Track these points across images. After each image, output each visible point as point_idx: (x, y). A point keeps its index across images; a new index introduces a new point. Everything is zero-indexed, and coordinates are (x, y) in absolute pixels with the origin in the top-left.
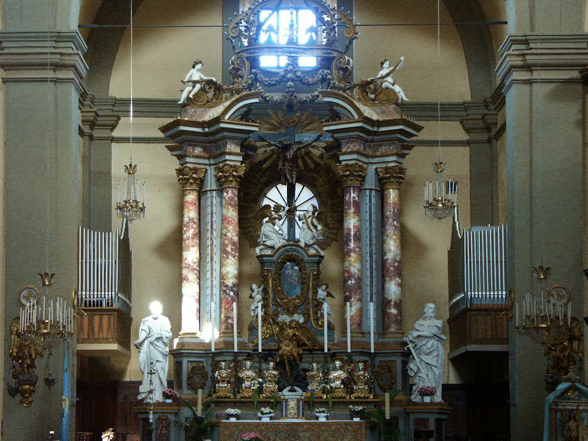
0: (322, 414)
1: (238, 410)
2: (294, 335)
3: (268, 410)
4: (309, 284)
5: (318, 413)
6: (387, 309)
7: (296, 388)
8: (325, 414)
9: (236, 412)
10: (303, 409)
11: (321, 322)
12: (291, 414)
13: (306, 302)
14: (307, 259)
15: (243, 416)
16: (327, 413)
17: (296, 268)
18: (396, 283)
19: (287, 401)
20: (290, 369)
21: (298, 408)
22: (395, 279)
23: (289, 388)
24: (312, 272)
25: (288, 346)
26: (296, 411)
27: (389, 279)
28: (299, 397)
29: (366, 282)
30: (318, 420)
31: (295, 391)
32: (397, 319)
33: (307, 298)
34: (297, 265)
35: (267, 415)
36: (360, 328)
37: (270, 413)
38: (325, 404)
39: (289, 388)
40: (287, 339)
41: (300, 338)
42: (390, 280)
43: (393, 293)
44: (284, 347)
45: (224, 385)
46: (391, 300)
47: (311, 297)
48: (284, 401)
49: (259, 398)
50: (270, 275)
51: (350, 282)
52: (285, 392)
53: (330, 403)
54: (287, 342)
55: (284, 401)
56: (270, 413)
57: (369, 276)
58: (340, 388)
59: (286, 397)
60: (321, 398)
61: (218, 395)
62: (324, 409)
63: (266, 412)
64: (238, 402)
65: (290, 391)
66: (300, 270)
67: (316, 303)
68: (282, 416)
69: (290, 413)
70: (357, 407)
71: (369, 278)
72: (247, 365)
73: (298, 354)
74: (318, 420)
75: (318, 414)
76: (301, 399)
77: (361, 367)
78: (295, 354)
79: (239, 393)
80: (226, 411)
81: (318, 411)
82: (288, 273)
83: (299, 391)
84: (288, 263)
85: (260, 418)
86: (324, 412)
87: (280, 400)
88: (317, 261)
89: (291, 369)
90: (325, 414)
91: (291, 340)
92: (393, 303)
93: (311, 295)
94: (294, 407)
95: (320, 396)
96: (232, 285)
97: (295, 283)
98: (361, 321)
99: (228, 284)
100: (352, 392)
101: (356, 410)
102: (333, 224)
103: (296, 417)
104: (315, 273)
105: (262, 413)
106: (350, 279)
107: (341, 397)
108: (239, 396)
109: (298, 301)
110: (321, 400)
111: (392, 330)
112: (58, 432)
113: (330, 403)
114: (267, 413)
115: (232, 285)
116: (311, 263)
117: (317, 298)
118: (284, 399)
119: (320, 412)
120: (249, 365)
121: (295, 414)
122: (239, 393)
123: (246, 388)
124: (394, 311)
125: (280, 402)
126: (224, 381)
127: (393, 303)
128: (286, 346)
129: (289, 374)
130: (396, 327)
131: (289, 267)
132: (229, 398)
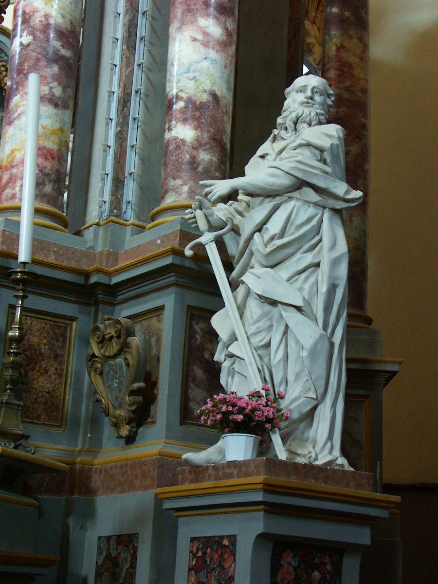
18: (200, 37)
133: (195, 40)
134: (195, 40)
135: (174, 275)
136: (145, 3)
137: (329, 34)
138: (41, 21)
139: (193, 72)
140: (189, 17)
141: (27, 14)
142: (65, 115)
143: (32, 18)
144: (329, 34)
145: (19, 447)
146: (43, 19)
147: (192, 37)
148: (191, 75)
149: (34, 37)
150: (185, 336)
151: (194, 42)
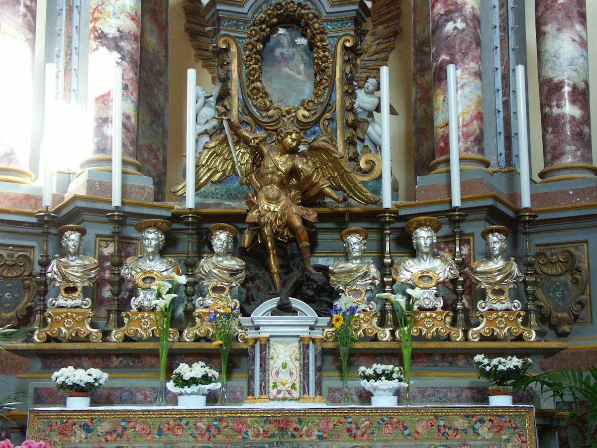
0: (383, 383)
1: (96, 372)
2: (293, 172)
3: (198, 370)
4: (334, 71)
5: (368, 378)
6: (551, 107)
7: (296, 303)
8: (395, 384)
9: (90, 380)
10: (318, 369)
11: (367, 162)
12: (280, 387)
13: (328, 115)
14: (329, 10)
15: (125, 396)
16: (400, 380)
17: (302, 41)
18: (577, 38)
19: (265, 345)
20: (281, 267)
21: (305, 367)
22: (572, 26)
23: (272, 303)
24: (341, 41)
25: (276, 200)
26: (297, 379)
27: (556, 26)
28: (304, 332)
29: (492, 40)
30: (176, 404)
31: (294, 312)
32: (581, 131)
33: (328, 106)
34: (304, 35)
35: (194, 388)
36: (481, 151)
37: (206, 379)
38: (392, 355)
39: (272, 303)
40: (272, 182)
41: (310, 177)
42: (559, 30)
43: (566, 63)
44: (264, 204)
45: (70, 303)
46: (562, 82)
47: (338, 103)
48: (258, 346)
49: (181, 339)
50: (234, 49)
51: (450, 26)
52: (262, 313)
53: (407, 353)
54: (273, 190)
55: (258, 346)
56: (206, 379)
57: (497, 24)
58: (433, 309)
59: (264, 333)
60: (375, 339)
61: (53, 331)
62: (391, 367)
63: (192, 375)
64: (118, 353)
65: (274, 312)
66: (311, 46)
67: (351, 118)
68: (251, 392)
69: (275, 385)
70: (503, 360)
71: (498, 29)
72: (146, 242)
73: (305, 222)
74: (66, 407)
75: (365, 384)
76: (314, 340)
77: (497, 246)
78: (298, 223)
79: (120, 324)
80: (56, 374)
81: (369, 371)
82: (282, 54)
83: (307, 312)
84: (281, 31)
85: (174, 399)
86: (389, 377)
87: (245, 346)
88: (354, 14)
89: (286, 268)
90: (395, 384)
91: (283, 185)
92: (567, 89)
93: (338, 97)
94: (290, 364)
95: (371, 333)
96: (117, 34)
97: (299, 77)
98: (482, 133)
99: (106, 31)
100: (469, 324)
101: (501, 367)
102: (378, 44)
103: (296, 394)
104: (348, 44)
105: (182, 382)
106: (451, 19)
107: (437, 338)
108: (116, 335)
109: (306, 113)
110: (375, 345)
111: (568, 160)
112: (590, 391)
113: (407, 353)
114: (193, 381)
115: (117, 34)
116: (337, 21)
117: (356, 106)
118: (256, 340)
119: (377, 377)
120: (154, 243)
121: (293, 386)
122: (120, 324)
123: (140, 309)
124: (569, 109)
125: (244, 353)
126: (74, 289)
127: (567, 89)
128: (269, 200)
129: (276, 279)
130: (579, 153)
131: (285, 41)
132: (87, 339)
133: (574, 41)
134: (574, 41)
135: (343, 256)
136: (511, 4)
137: (362, 37)
138: (470, 12)
139: (575, 65)
140: (568, 23)
141: (459, 5)
142: (213, 90)
143: (464, 8)
144: (362, 37)
145: (254, 341)
146: (471, 10)
147: (572, 38)
148: (575, 68)
149: (467, 25)
150: (130, 378)
151: (574, 42)
